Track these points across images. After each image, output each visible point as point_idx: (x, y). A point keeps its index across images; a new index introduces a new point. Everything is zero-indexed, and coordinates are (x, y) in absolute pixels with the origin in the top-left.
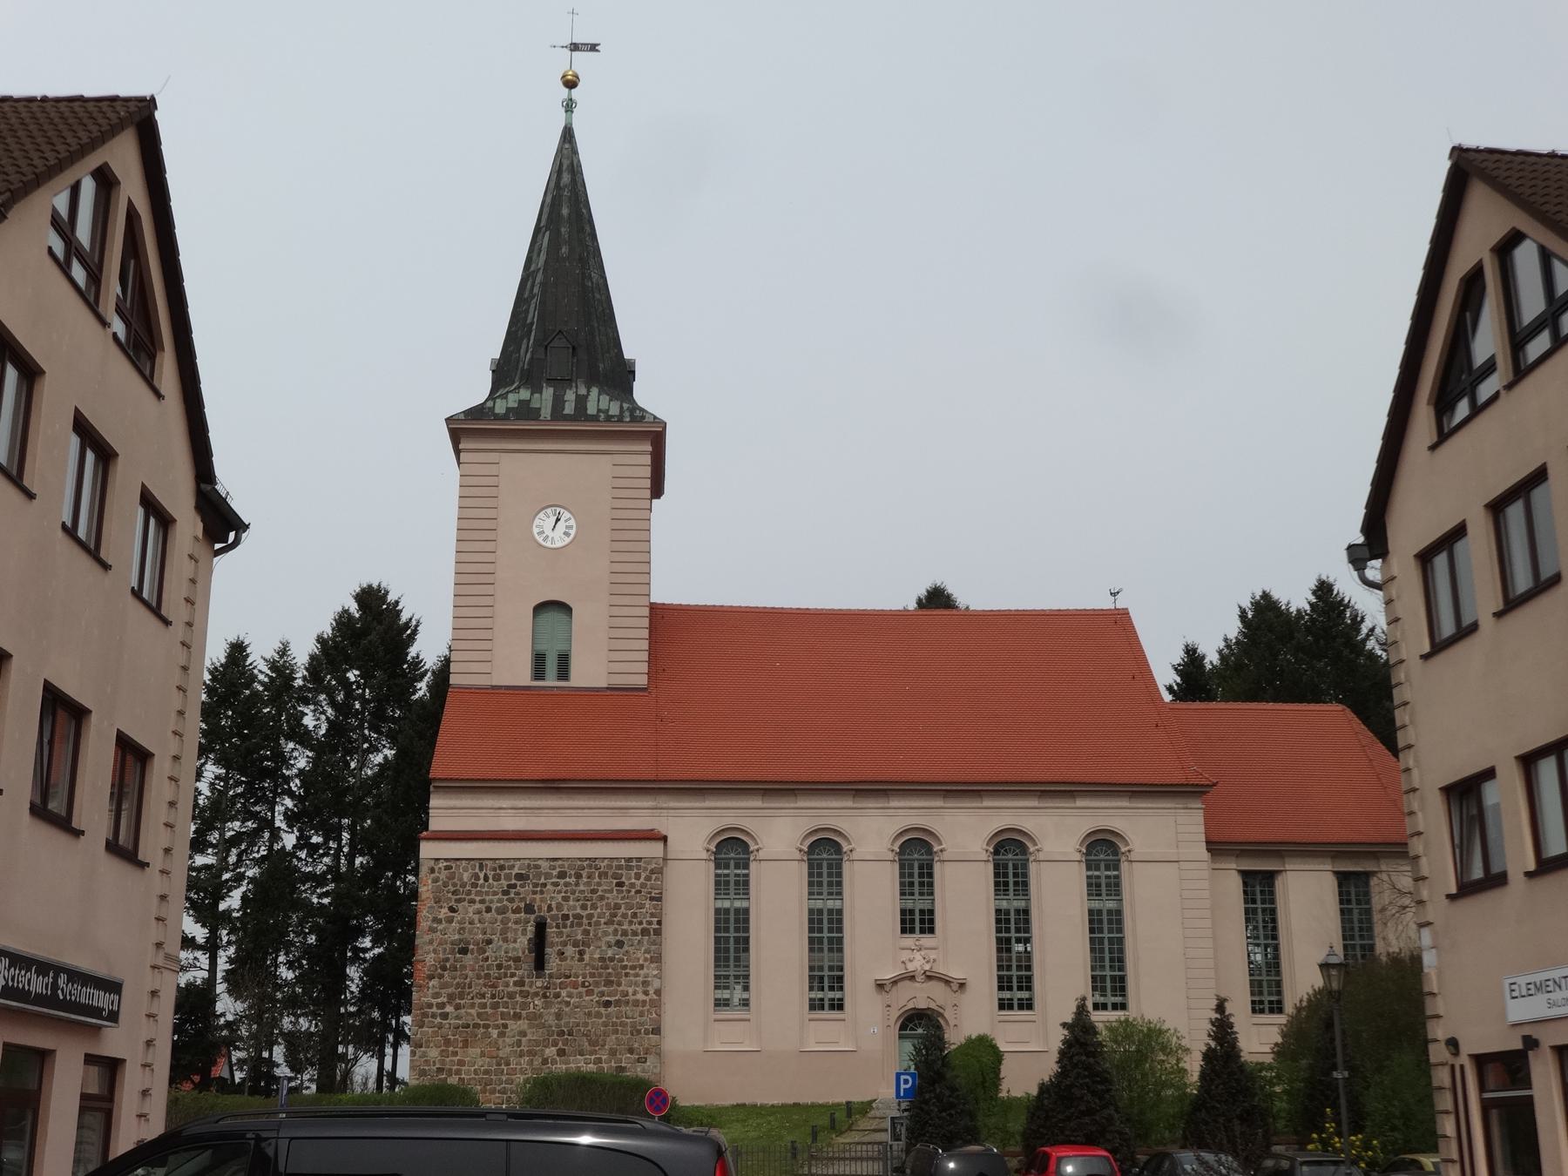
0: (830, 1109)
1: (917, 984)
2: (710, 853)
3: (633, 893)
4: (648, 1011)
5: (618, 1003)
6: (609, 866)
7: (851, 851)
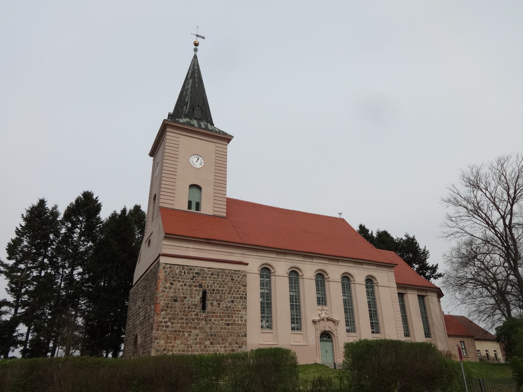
5: (232, 324)
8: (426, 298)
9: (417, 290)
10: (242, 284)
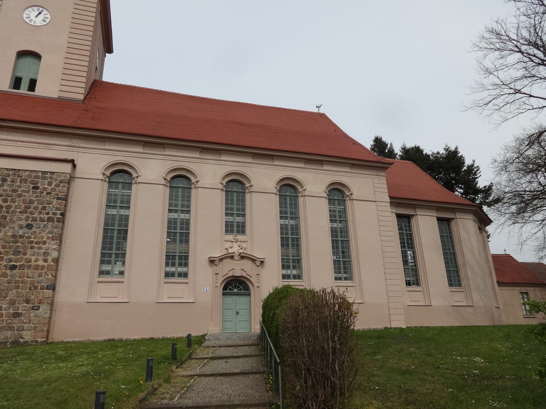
0: (174, 343)
1: (235, 262)
2: (105, 176)
3: (45, 194)
4: (45, 273)
5: (22, 267)
6: (30, 176)
7: (197, 182)
8: (454, 222)
9: (437, 210)
10: (56, 196)
